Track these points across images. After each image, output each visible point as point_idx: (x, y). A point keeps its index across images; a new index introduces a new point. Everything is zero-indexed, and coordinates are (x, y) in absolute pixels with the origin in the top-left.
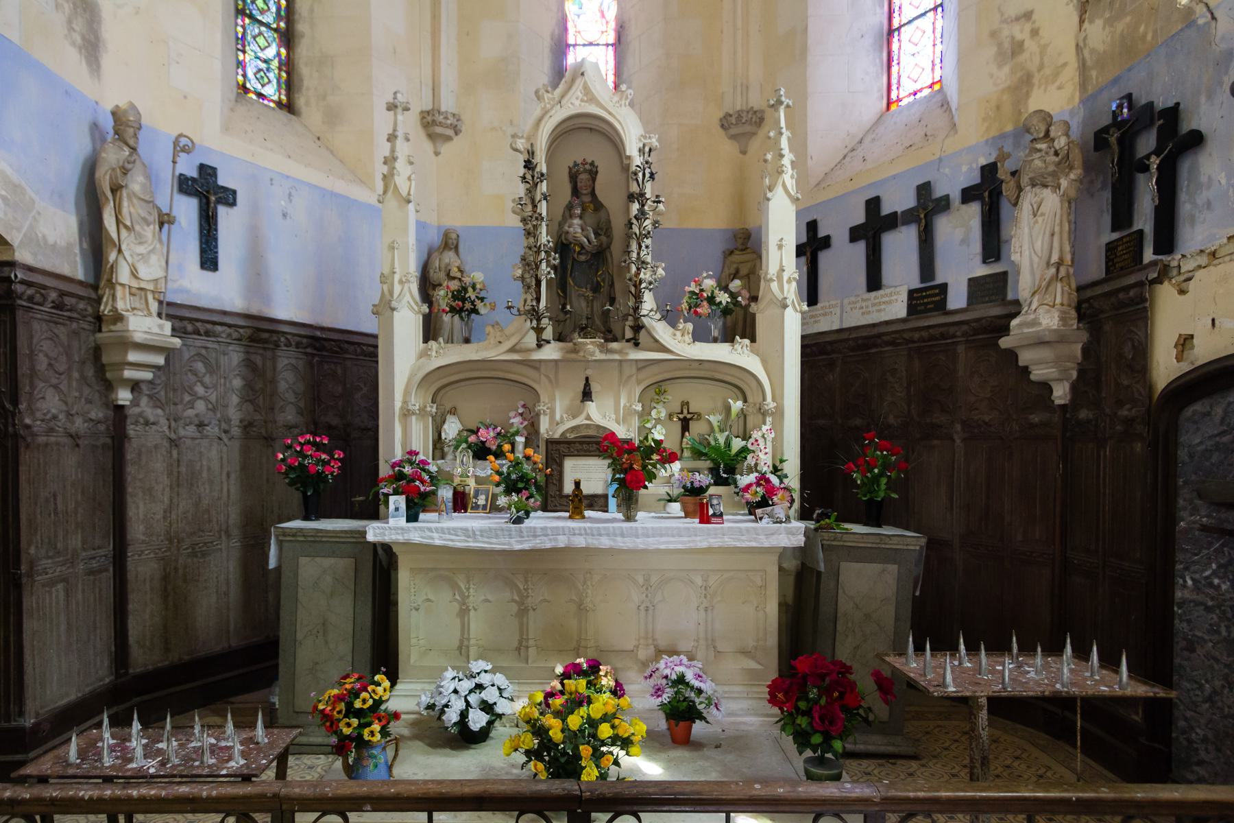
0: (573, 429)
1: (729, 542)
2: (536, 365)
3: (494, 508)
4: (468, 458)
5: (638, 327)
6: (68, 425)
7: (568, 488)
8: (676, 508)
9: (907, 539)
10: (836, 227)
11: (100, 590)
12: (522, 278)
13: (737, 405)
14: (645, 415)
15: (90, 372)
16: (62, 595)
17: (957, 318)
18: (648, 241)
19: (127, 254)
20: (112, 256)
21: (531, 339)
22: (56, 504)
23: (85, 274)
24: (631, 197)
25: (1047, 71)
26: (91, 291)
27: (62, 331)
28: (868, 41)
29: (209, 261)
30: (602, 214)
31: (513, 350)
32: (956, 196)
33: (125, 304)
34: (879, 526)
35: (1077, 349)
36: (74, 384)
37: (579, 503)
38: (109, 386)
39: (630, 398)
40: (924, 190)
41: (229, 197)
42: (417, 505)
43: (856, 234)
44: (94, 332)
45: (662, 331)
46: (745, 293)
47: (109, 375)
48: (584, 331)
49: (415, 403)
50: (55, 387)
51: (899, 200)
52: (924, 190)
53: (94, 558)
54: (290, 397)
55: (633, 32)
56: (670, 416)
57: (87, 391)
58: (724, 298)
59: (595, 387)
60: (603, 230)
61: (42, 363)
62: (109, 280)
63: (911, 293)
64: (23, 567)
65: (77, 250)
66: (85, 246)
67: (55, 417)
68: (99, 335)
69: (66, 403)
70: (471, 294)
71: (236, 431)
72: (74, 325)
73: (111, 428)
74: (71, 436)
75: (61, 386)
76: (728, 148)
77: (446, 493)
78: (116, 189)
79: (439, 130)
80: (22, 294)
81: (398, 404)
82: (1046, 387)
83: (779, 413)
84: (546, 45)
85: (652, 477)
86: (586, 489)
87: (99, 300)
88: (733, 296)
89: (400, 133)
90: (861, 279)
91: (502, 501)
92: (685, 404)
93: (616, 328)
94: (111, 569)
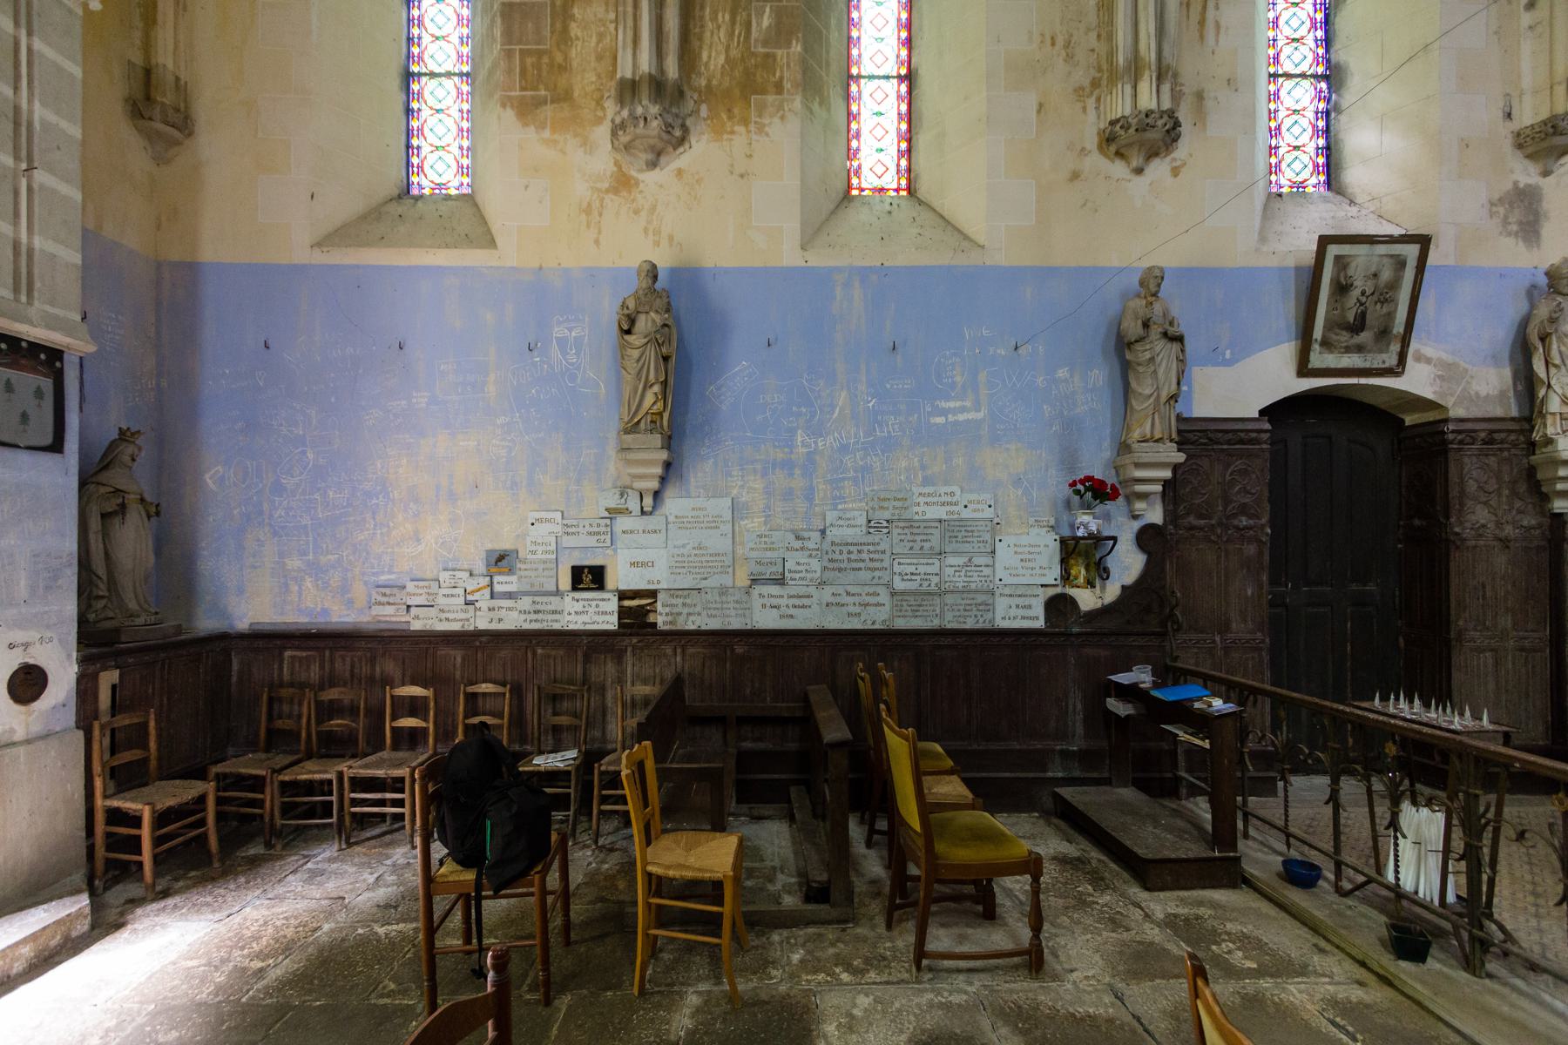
6: (1497, 532)
11: (1533, 667)
15: (1522, 487)
16: (1490, 661)
19: (1556, 387)
20: (1542, 393)
22: (1484, 592)
23: (1520, 411)
26: (1524, 423)
27: (1492, 461)
33: (1556, 428)
36: (1504, 499)
38: (1545, 498)
44: (1528, 456)
47: (1544, 489)
50: (1485, 503)
53: (1525, 638)
57: (1518, 504)
61: (1472, 486)
62: (1541, 412)
64: (1452, 633)
65: (1511, 394)
66: (1520, 388)
67: (1483, 526)
68: (1532, 458)
69: (1496, 516)
72: (1506, 454)
73: (1547, 533)
74: (1501, 540)
75: (1491, 502)
78: (1544, 338)
80: (1454, 440)
94: (1548, 651)
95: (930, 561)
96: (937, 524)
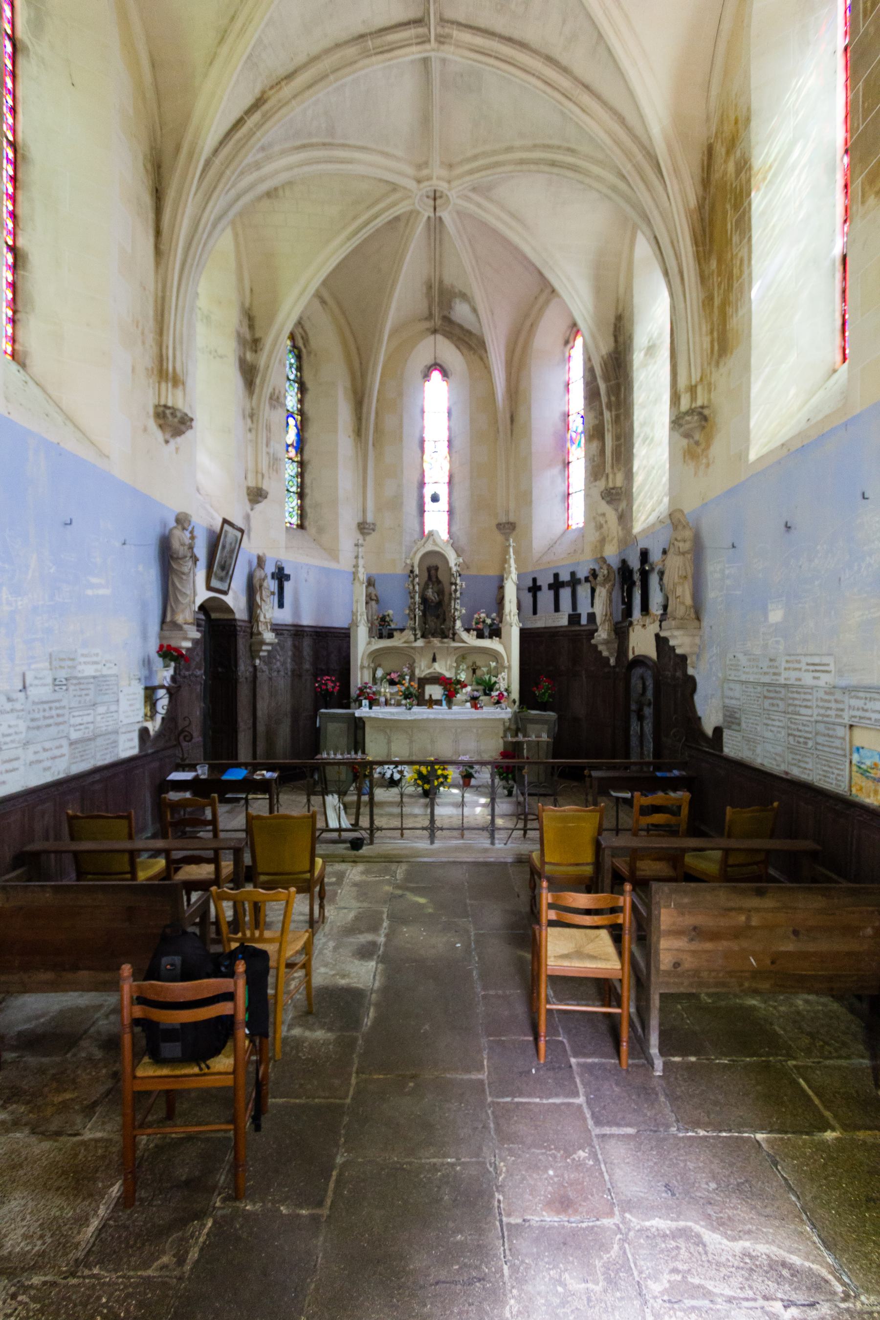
0: (429, 674)
1: (484, 716)
2: (414, 648)
3: (399, 704)
4: (386, 685)
5: (454, 634)
7: (427, 697)
8: (468, 704)
9: (552, 715)
10: (545, 581)
12: (409, 614)
13: (493, 664)
14: (457, 668)
17: (583, 628)
18: (458, 601)
21: (412, 638)
24: (452, 584)
25: (610, 538)
28: (559, 498)
29: (281, 605)
30: (440, 586)
31: (405, 642)
32: (583, 579)
34: (545, 710)
35: (616, 645)
37: (432, 703)
39: (451, 661)
40: (573, 574)
41: (288, 577)
42: (373, 703)
43: (550, 587)
45: (464, 635)
46: (498, 619)
48: (434, 636)
49: (366, 664)
51: (565, 577)
52: (573, 574)
54: (307, 658)
55: (456, 480)
56: (468, 668)
58: (489, 621)
59: (438, 657)
60: (440, 592)
63: (570, 616)
70: (388, 619)
71: (289, 673)
76: (499, 538)
77: (383, 699)
79: (366, 531)
81: (359, 663)
82: (608, 659)
83: (509, 668)
84: (415, 485)
85: (458, 693)
86: (434, 697)
87: (252, 627)
88: (493, 620)
89: (360, 555)
90: (552, 606)
91: (404, 702)
92: (474, 663)
93: (447, 633)
95: (89, 712)
96: (92, 680)
